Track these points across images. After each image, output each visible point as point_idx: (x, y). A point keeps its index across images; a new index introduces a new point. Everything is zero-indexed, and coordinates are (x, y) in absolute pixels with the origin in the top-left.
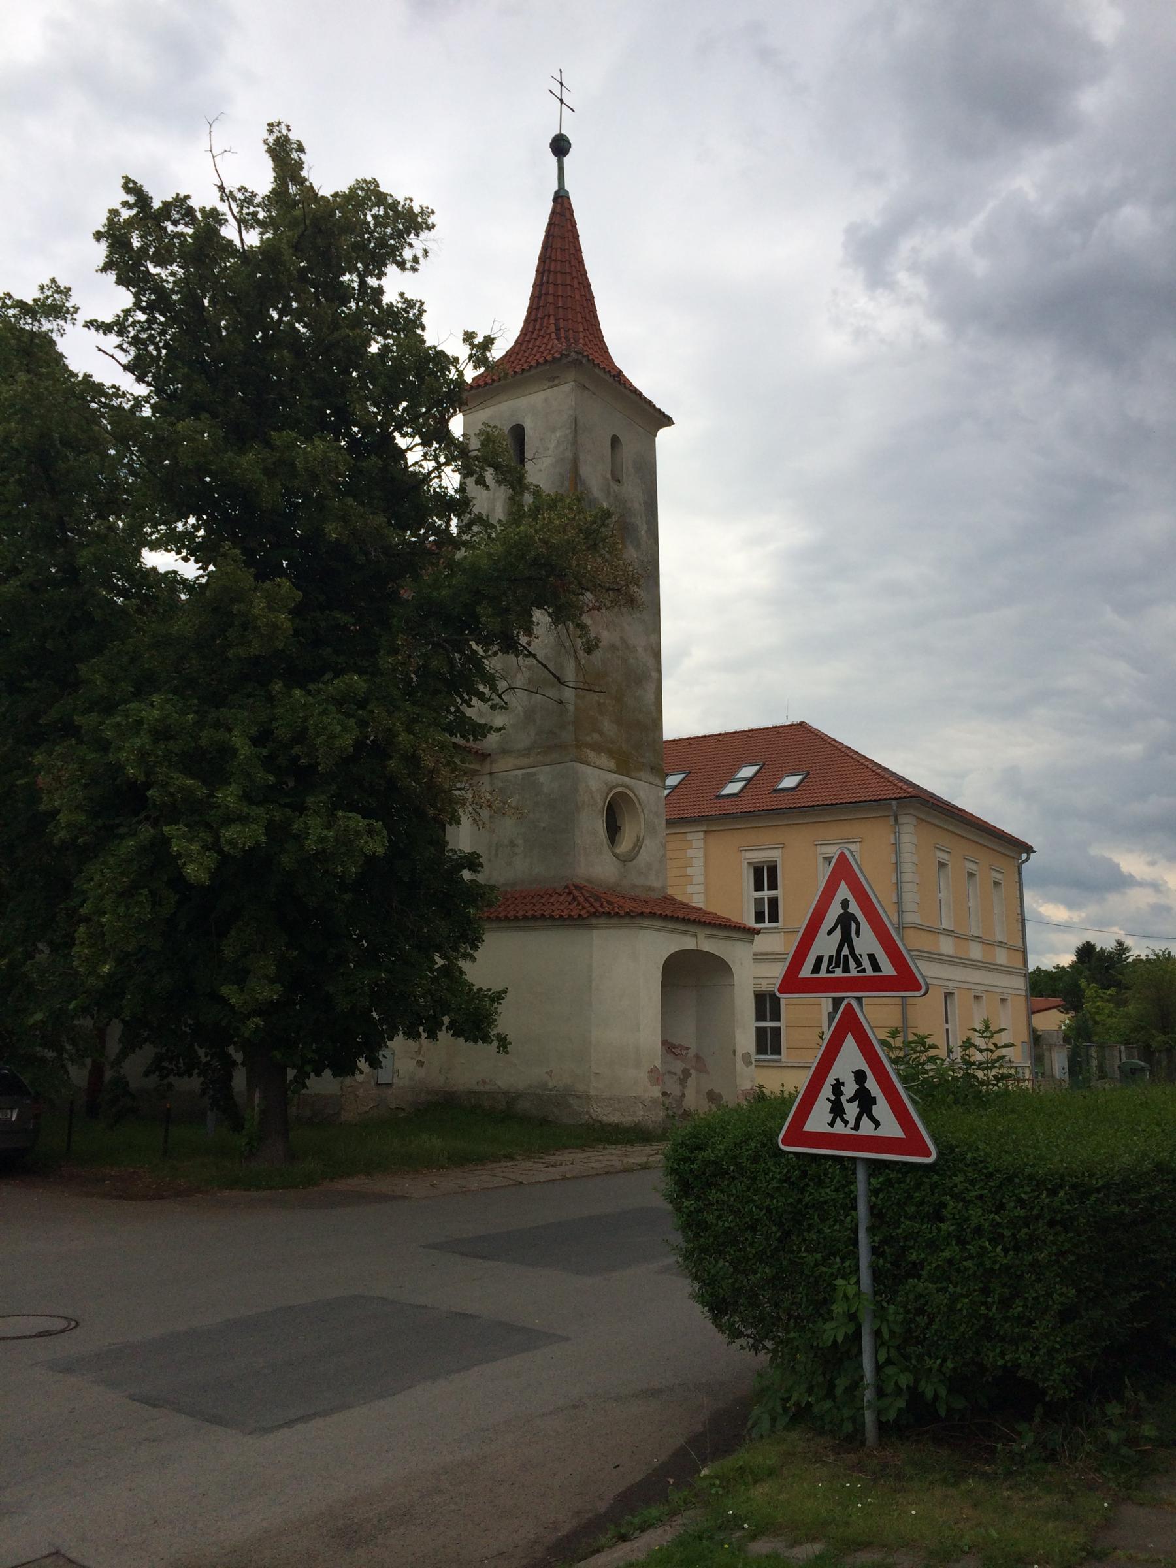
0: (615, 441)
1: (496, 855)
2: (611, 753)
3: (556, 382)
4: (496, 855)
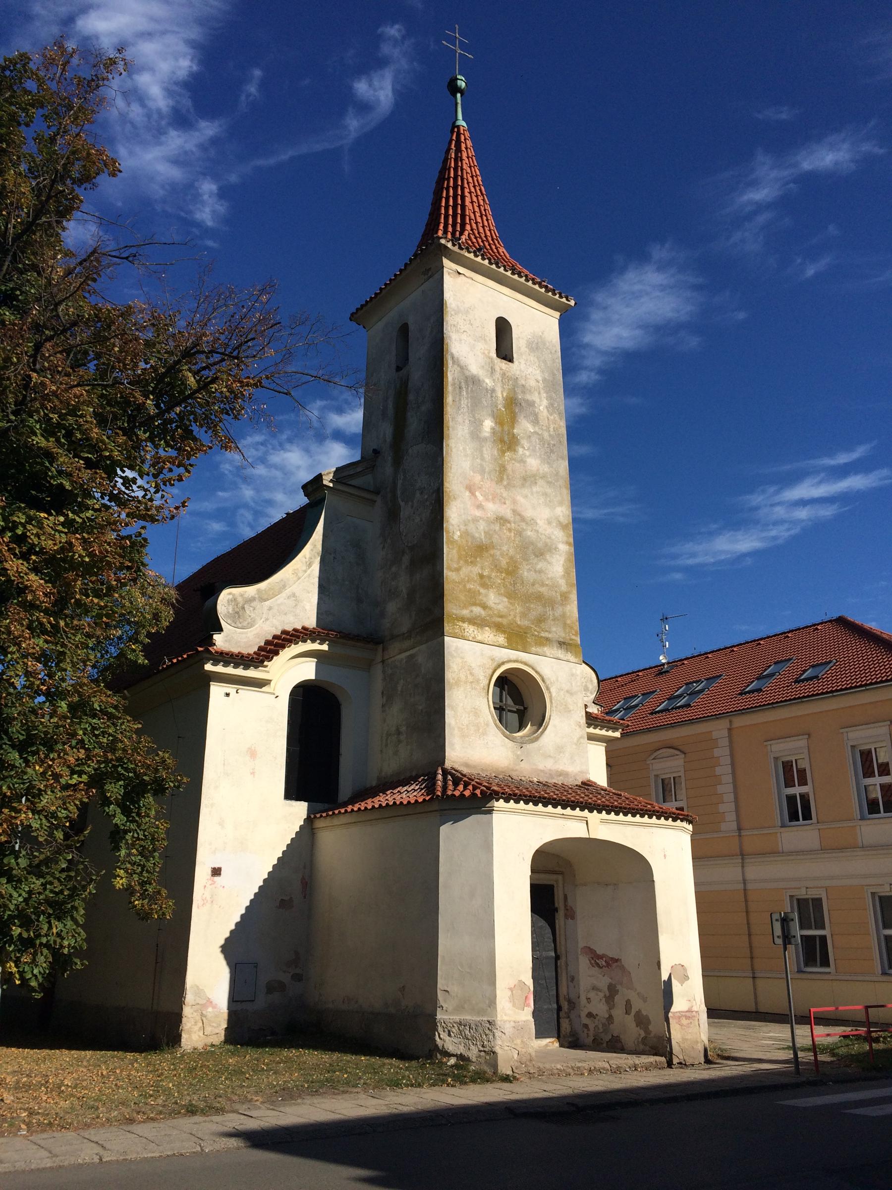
0: (503, 328)
1: (387, 745)
2: (499, 628)
3: (430, 273)
4: (387, 745)
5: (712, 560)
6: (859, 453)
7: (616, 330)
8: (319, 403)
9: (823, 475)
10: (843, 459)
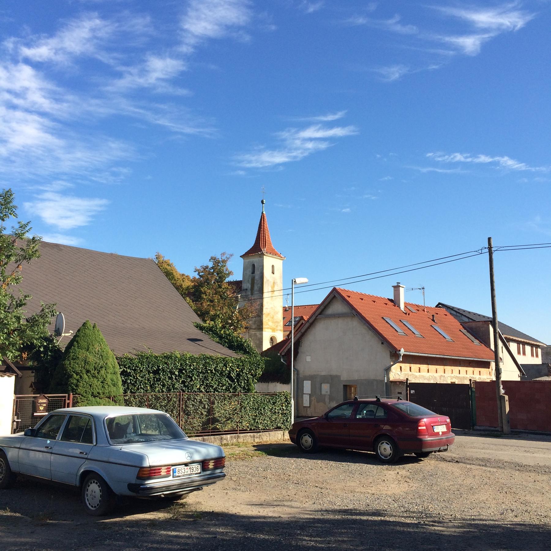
2: (271, 329)
5: (261, 166)
6: (339, 115)
7: (203, 24)
8: (13, 39)
9: (320, 125)
10: (330, 118)
